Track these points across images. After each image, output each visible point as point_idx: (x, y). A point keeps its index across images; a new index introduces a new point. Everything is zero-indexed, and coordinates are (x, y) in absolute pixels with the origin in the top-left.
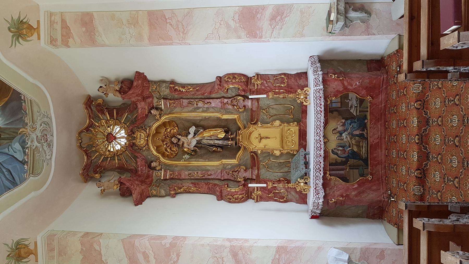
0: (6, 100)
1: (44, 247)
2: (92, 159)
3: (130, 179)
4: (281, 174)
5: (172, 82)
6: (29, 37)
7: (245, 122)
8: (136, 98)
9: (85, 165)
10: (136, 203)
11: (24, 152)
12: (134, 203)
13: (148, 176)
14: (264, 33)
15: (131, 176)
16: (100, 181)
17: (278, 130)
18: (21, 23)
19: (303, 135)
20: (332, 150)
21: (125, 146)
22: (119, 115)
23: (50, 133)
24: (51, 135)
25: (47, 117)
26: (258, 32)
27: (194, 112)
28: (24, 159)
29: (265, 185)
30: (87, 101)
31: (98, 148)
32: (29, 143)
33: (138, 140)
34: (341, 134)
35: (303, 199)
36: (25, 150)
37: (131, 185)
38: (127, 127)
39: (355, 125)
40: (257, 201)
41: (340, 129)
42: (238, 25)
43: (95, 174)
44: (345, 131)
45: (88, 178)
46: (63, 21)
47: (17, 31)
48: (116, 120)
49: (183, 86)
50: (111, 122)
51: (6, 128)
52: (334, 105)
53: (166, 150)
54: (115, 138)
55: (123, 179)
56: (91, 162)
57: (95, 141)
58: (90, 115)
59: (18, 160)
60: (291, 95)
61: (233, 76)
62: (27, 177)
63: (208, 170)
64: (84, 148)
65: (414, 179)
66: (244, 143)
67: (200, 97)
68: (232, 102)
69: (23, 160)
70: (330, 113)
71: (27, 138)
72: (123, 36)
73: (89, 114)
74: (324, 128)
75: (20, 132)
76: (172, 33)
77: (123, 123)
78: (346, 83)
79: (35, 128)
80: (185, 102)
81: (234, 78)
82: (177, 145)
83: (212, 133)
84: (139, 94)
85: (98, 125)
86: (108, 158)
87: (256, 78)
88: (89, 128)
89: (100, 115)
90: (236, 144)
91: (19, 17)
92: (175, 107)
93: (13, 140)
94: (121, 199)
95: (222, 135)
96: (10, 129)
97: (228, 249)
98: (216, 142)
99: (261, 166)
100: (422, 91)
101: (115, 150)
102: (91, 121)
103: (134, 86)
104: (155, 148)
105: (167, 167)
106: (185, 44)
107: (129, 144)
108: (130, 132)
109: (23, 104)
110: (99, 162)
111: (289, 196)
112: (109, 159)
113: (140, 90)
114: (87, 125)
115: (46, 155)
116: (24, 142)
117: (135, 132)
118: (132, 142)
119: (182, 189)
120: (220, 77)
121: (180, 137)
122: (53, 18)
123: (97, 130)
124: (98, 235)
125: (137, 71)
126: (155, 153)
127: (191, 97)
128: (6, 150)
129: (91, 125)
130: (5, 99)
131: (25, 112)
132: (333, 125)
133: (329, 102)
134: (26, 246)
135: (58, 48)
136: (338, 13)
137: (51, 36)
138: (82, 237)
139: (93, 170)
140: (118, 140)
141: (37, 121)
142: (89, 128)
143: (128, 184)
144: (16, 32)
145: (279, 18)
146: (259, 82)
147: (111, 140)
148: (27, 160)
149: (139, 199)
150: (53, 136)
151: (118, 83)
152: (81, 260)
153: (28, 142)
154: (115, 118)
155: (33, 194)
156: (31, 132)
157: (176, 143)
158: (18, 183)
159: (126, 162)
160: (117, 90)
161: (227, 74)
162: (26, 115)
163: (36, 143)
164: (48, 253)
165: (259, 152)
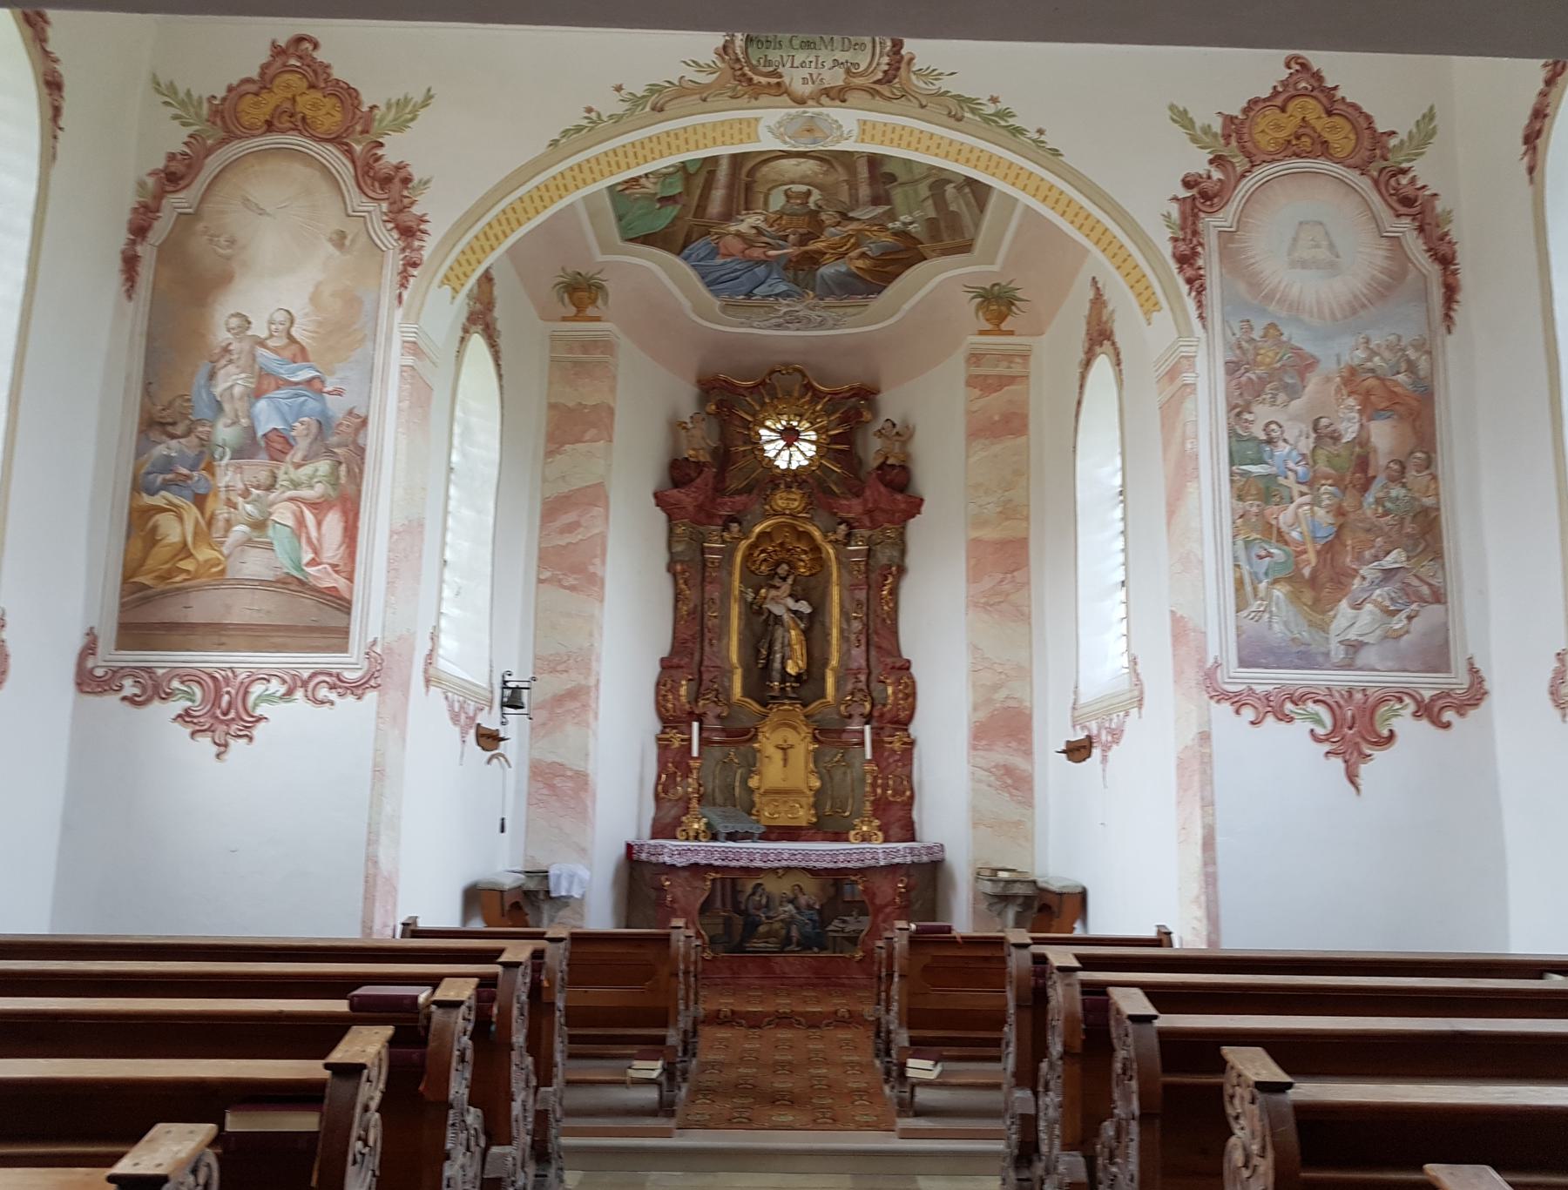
4: (710, 787)
5: (902, 570)
6: (984, 314)
7: (818, 717)
13: (711, 518)
14: (982, 753)
17: (802, 786)
19: (790, 833)
20: (760, 885)
26: (984, 742)
27: (841, 610)
28: (755, 295)
29: (695, 753)
33: (784, 495)
34: (791, 901)
35: (663, 829)
39: (809, 929)
40: (659, 739)
41: (803, 900)
42: (998, 705)
44: (797, 908)
46: (1012, 379)
49: (894, 592)
52: (847, 888)
53: (762, 552)
60: (868, 806)
61: (910, 694)
63: (720, 640)
65: (715, 1007)
66: (774, 716)
67: (871, 624)
68: (861, 690)
70: (831, 882)
74: (804, 868)
76: (987, 583)
78: (888, 910)
80: (861, 595)
81: (907, 696)
82: (773, 574)
83: (797, 647)
87: (906, 740)
89: (837, 415)
90: (773, 698)
92: (850, 573)
94: (666, 460)
95: (791, 669)
97: (583, 682)
98: (778, 656)
99: (726, 749)
100: (866, 1020)
104: (768, 530)
105: (729, 554)
106: (967, 607)
111: (668, 804)
116: (789, 296)
119: (683, 586)
120: (908, 668)
121: (790, 581)
122: (1018, 360)
126: (758, 529)
127: (872, 607)
129: (817, 396)
132: (810, 885)
133: (853, 878)
134: (594, 302)
136: (1008, 882)
145: (1009, 781)
146: (897, 745)
155: (687, 304)
157: (776, 573)
161: (914, 682)
163: (784, 310)
165: (756, 745)
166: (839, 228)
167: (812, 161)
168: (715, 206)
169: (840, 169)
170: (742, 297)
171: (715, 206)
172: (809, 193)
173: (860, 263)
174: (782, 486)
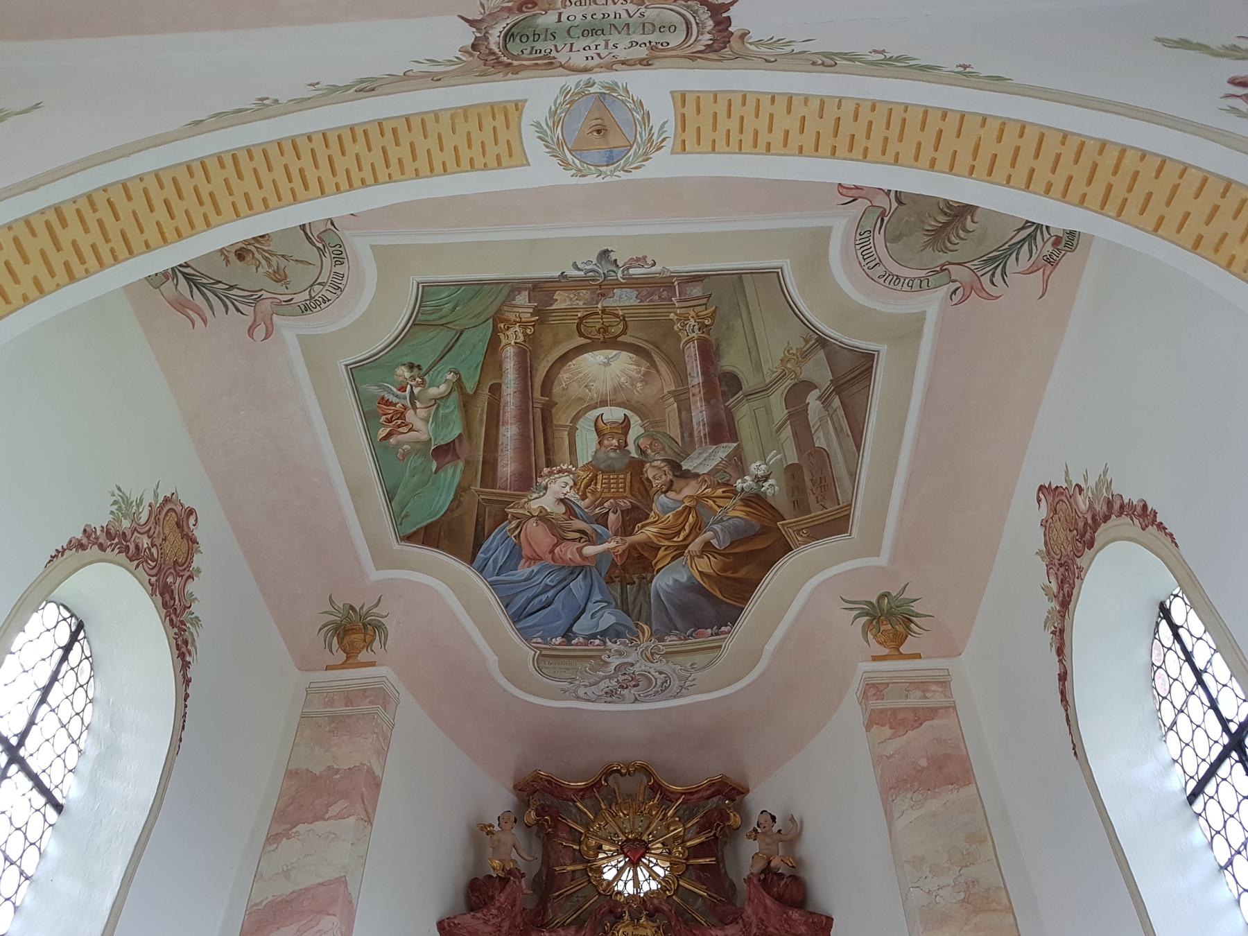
0: (714, 593)
1: (358, 681)
2: (576, 800)
3: (518, 903)
6: (875, 636)
8: (754, 920)
9: (562, 785)
10: (446, 925)
11: (594, 636)
12: (447, 919)
15: (524, 909)
16: (515, 822)
18: (906, 620)
21: (614, 891)
22: (701, 874)
23: (641, 695)
24: (637, 696)
25: (681, 686)
28: (576, 635)
30: (730, 786)
31: (607, 815)
32: (615, 647)
36: (597, 638)
37: (498, 909)
38: (669, 897)
43: (536, 810)
45: (525, 793)
46: (933, 712)
47: (885, 611)
48: (685, 865)
50: (680, 849)
51: (649, 595)
54: (634, 863)
55: (517, 883)
56: (569, 800)
57: (625, 810)
58: (693, 795)
59: (575, 621)
62: (534, 643)
64: (606, 781)
69: (575, 633)
71: (627, 642)
72: (928, 870)
73: (697, 791)
75: (641, 626)
77: (679, 885)
79: (652, 660)
84: (767, 927)
85: (669, 814)
86: (580, 845)
88: (659, 793)
89: (695, 821)
91: (918, 615)
93: (623, 611)
94: (463, 881)
96: (647, 603)
101: (601, 862)
102: (679, 796)
103: (787, 910)
107: (617, 903)
108: (651, 904)
109: (709, 631)
110: (569, 820)
112: (575, 847)
113: (778, 930)
114: (667, 788)
115: (585, 686)
116: (619, 635)
117: (655, 922)
118: (625, 912)
122: (934, 687)
123: (654, 813)
124: (370, 810)
125: (833, 919)
128: (597, 596)
129: (667, 798)
130: (718, 591)
131: (691, 635)
135: (860, 704)
137: (888, 684)
138: (370, 772)
139: (549, 806)
140: (629, 871)
141: (670, 664)
142: (659, 793)
143: (502, 900)
144: (881, 610)
147: (628, 851)
148: (573, 642)
149: (458, 932)
150: (634, 703)
151: (791, 865)
152: (310, 769)
153: (618, 643)
154: (692, 862)
155: (492, 659)
156: (642, 651)
158: (520, 625)
159: (566, 896)
160: (769, 862)
162: (683, 638)
163: (615, 662)
164: (343, 691)
166: (671, 494)
167: (624, 355)
168: (508, 466)
169: (663, 368)
170: (559, 640)
171: (508, 466)
172: (626, 425)
173: (704, 564)
174: (626, 917)
